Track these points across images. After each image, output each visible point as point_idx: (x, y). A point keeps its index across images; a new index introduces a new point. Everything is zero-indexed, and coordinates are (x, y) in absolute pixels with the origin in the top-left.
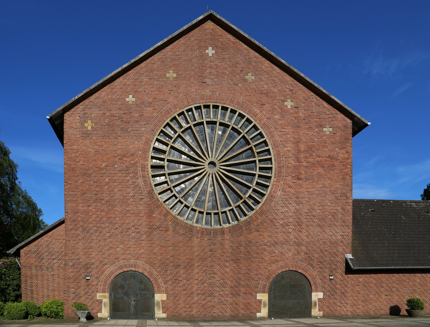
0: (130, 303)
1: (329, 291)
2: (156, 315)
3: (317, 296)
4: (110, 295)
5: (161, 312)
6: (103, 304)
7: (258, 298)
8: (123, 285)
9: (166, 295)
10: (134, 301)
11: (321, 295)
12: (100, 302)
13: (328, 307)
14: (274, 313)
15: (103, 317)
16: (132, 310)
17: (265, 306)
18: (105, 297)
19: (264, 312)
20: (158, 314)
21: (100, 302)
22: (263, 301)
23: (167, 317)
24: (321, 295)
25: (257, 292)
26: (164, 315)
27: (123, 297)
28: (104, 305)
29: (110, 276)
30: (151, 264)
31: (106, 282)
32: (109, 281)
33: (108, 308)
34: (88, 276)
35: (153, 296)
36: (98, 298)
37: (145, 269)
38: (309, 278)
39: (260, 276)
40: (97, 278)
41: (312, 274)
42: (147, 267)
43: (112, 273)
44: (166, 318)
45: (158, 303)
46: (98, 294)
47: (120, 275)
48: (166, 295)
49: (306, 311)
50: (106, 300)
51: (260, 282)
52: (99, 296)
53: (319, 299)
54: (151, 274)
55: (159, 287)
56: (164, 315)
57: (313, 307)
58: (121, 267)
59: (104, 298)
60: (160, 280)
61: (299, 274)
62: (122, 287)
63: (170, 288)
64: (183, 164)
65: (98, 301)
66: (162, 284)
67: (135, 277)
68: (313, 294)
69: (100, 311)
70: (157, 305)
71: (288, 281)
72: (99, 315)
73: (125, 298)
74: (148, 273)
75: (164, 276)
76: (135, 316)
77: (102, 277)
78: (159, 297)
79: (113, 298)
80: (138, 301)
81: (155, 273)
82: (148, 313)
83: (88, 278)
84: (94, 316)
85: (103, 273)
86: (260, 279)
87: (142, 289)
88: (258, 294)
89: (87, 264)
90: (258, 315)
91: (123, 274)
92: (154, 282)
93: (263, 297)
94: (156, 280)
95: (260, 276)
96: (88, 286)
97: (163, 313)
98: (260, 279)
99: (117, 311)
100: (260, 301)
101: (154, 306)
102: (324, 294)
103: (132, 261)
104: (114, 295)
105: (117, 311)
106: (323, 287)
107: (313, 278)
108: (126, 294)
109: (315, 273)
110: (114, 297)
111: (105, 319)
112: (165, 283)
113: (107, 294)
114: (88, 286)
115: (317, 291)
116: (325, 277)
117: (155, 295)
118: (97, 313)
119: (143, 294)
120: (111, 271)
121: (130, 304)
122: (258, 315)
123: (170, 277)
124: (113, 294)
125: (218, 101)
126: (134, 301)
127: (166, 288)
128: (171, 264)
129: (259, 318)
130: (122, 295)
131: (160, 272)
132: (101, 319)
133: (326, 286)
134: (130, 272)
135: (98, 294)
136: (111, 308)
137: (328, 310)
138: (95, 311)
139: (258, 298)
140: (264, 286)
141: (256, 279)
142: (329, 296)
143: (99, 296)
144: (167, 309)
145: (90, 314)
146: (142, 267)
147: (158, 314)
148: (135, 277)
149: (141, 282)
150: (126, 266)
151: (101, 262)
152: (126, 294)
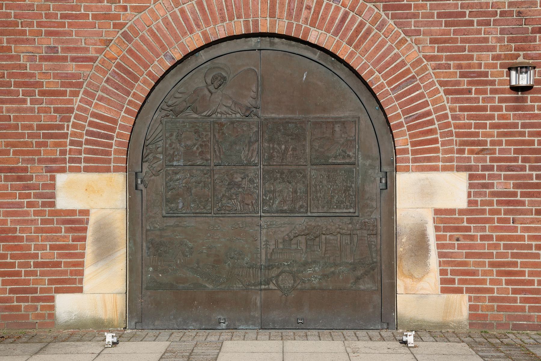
1: (508, 165)
3: (426, 192)
7: (63, 202)
9: (464, 176)
11: (452, 190)
13: (505, 270)
14: (163, 294)
17: (105, 252)
19: (102, 288)
22: (92, 219)
24: (452, 190)
25: (56, 166)
28: (98, 240)
38: (377, 80)
39: (72, 68)
41: (394, 54)
49: (366, 285)
51: (77, 102)
53: (445, 218)
57: (403, 266)
61: (317, 55)
64: (375, 94)
68: (405, 182)
71: (248, 101)
78: (426, 195)
86: (73, 83)
88: (61, 179)
90: (66, 306)
93: (96, 196)
95: (72, 68)
98: (73, 83)
100: (76, 222)
102: (477, 185)
106: (470, 141)
107: (400, 75)
109: (414, 54)
115: (426, 162)
116: (479, 78)
122: (66, 306)
129: (67, 326)
133: (488, 135)
137: (502, 287)
139: (63, 202)
140: (103, 130)
141: (51, 83)
142: (507, 199)
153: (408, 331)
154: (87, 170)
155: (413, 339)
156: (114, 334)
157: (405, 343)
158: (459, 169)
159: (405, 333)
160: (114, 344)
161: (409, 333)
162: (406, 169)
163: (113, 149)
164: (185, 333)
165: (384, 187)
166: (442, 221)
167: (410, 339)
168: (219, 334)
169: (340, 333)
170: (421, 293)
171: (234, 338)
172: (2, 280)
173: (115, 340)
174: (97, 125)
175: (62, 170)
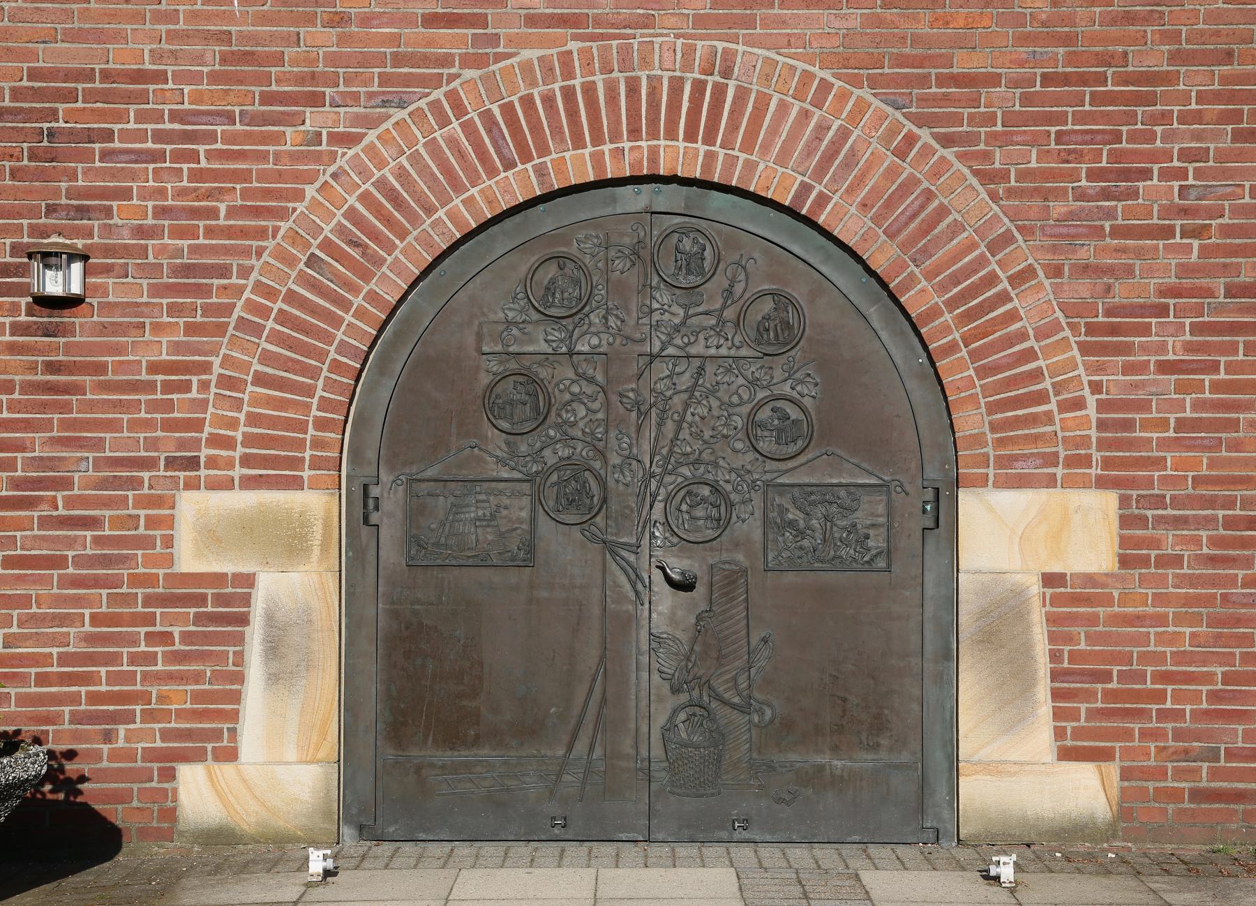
0: (627, 623)
2: (967, 786)
4: (363, 510)
5: (1039, 737)
6: (255, 635)
8: (531, 381)
9: (1108, 501)
10: (684, 586)
12: (221, 607)
15: (247, 815)
16: (653, 705)
18: (288, 542)
20: (995, 768)
21: (221, 607)
23: (1124, 813)
26: (1085, 791)
27: (530, 547)
28: (273, 649)
29: (359, 245)
30: (933, 91)
31: (303, 330)
32: (352, 329)
33: (323, 686)
34: (48, 258)
35: (941, 520)
36: (189, 560)
37: (831, 155)
40: (191, 278)
42: (870, 122)
43: (393, 206)
44: (1110, 832)
45: (1005, 613)
46: (194, 508)
47: (501, 240)
48: (1108, 501)
50: (300, 590)
52: (202, 526)
54: (924, 225)
55: (1018, 399)
56: (1085, 791)
58: (518, 133)
59: (275, 555)
60: (1033, 306)
62: (525, 399)
63: (1172, 402)
65: (187, 592)
66: (1064, 360)
67: (692, 263)
69: (210, 734)
70: (988, 638)
72: (199, 793)
73: (563, 546)
74: (881, 207)
75: (1087, 253)
76: (692, 801)
77: (266, 271)
78: (1021, 537)
79: (391, 553)
80: (730, 582)
81: (970, 202)
82: (864, 761)
83: (53, 284)
84: (117, 814)
85: (266, 207)
87: (786, 430)
89: (52, 86)
91: (545, 220)
92: (945, 329)
94: (977, 300)
96: (55, 385)
97: (1067, 754)
99: (452, 737)
101: (949, 655)
103: (665, 53)
104: (415, 512)
105: (439, 720)
108: (578, 495)
110: (414, 540)
111: (272, 851)
112: (1107, 335)
113: (316, 505)
114: (55, 385)
117: (970, 504)
118: (168, 762)
119: (808, 495)
120: (384, 181)
121: (618, 627)
123: (1164, 265)
124: (392, 498)
125: (781, 80)
126: (684, 586)
127: (1118, 418)
128: (1193, 81)
130: (520, 509)
131: (1039, 186)
132: (227, 851)
134: (634, 199)
135: (194, 508)
136: (371, 689)
138: (136, 737)
143: (202, 526)
144: (1127, 706)
145: (71, 785)
146: (802, 125)
147: (995, 768)
148: (692, 263)
149: (779, 333)
150: (580, 116)
151: (243, 62)
152: (578, 495)
153: (998, 853)
154: (249, 483)
155: (1012, 871)
156: (329, 852)
157: (997, 878)
158: (1102, 483)
159: (994, 859)
160: (327, 873)
161: (1003, 859)
162: (982, 482)
163: (308, 437)
164: (563, 851)
165: (930, 524)
166: (1055, 600)
167: (1007, 872)
168: (557, 853)
169: (778, 854)
170: (1016, 762)
171: (566, 861)
172: (5, 636)
173: (330, 864)
174: (302, 303)
175: (192, 485)
